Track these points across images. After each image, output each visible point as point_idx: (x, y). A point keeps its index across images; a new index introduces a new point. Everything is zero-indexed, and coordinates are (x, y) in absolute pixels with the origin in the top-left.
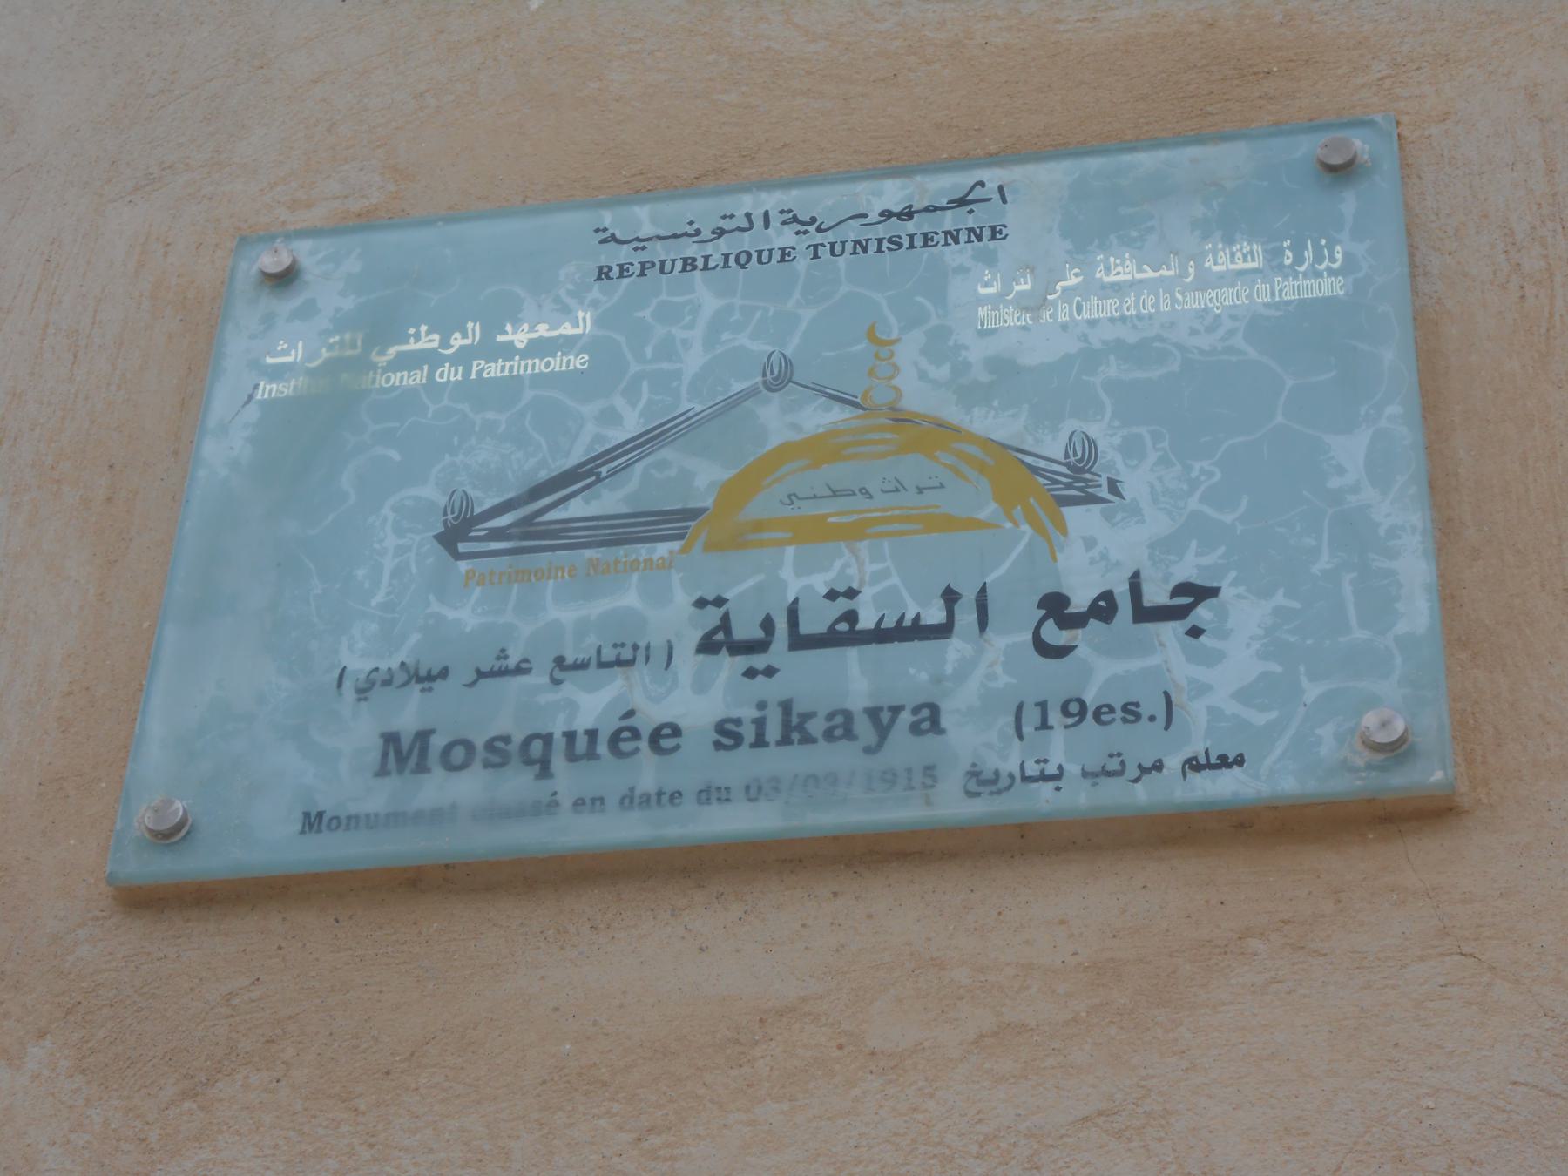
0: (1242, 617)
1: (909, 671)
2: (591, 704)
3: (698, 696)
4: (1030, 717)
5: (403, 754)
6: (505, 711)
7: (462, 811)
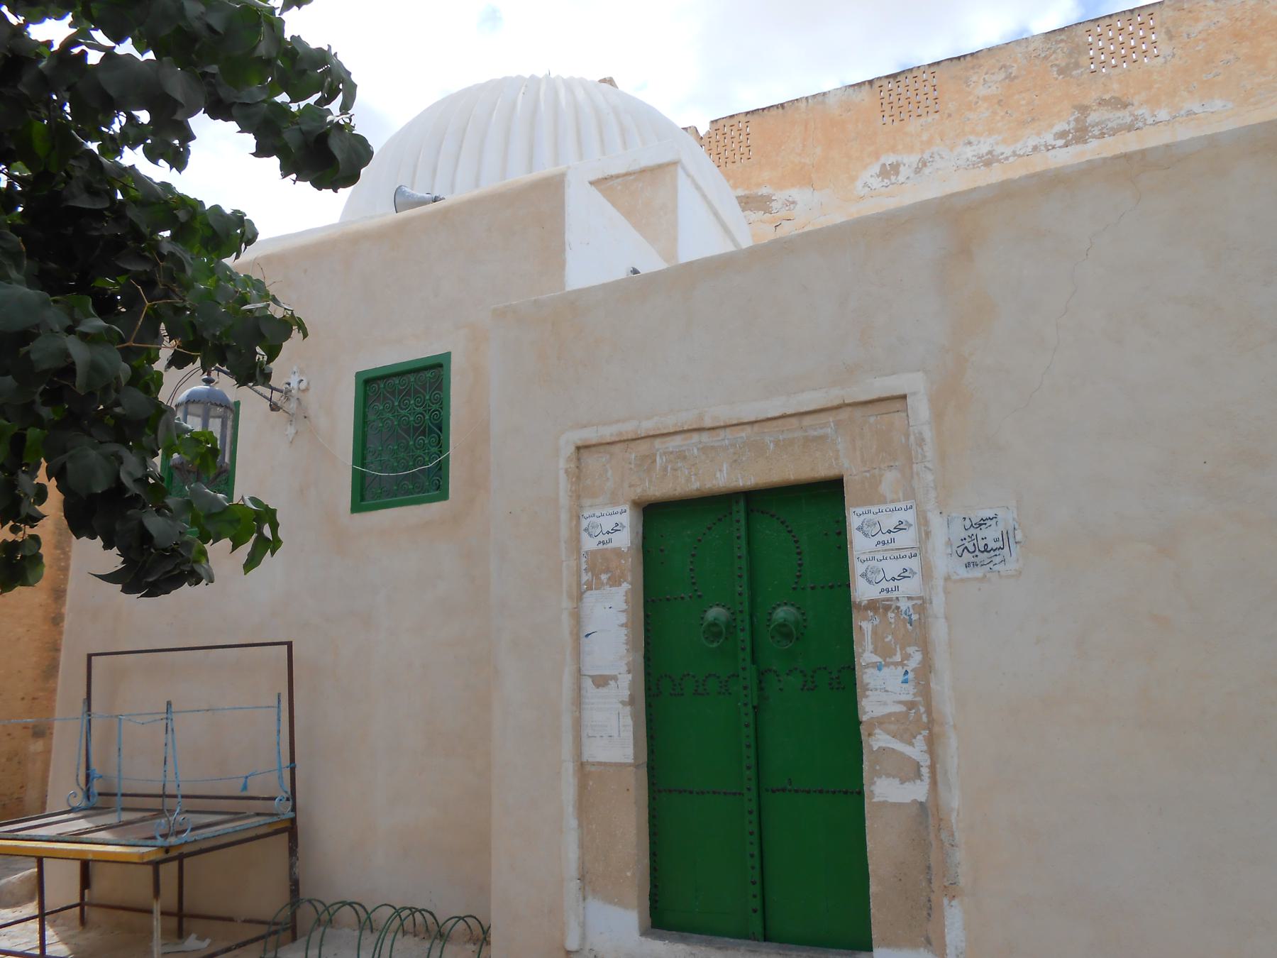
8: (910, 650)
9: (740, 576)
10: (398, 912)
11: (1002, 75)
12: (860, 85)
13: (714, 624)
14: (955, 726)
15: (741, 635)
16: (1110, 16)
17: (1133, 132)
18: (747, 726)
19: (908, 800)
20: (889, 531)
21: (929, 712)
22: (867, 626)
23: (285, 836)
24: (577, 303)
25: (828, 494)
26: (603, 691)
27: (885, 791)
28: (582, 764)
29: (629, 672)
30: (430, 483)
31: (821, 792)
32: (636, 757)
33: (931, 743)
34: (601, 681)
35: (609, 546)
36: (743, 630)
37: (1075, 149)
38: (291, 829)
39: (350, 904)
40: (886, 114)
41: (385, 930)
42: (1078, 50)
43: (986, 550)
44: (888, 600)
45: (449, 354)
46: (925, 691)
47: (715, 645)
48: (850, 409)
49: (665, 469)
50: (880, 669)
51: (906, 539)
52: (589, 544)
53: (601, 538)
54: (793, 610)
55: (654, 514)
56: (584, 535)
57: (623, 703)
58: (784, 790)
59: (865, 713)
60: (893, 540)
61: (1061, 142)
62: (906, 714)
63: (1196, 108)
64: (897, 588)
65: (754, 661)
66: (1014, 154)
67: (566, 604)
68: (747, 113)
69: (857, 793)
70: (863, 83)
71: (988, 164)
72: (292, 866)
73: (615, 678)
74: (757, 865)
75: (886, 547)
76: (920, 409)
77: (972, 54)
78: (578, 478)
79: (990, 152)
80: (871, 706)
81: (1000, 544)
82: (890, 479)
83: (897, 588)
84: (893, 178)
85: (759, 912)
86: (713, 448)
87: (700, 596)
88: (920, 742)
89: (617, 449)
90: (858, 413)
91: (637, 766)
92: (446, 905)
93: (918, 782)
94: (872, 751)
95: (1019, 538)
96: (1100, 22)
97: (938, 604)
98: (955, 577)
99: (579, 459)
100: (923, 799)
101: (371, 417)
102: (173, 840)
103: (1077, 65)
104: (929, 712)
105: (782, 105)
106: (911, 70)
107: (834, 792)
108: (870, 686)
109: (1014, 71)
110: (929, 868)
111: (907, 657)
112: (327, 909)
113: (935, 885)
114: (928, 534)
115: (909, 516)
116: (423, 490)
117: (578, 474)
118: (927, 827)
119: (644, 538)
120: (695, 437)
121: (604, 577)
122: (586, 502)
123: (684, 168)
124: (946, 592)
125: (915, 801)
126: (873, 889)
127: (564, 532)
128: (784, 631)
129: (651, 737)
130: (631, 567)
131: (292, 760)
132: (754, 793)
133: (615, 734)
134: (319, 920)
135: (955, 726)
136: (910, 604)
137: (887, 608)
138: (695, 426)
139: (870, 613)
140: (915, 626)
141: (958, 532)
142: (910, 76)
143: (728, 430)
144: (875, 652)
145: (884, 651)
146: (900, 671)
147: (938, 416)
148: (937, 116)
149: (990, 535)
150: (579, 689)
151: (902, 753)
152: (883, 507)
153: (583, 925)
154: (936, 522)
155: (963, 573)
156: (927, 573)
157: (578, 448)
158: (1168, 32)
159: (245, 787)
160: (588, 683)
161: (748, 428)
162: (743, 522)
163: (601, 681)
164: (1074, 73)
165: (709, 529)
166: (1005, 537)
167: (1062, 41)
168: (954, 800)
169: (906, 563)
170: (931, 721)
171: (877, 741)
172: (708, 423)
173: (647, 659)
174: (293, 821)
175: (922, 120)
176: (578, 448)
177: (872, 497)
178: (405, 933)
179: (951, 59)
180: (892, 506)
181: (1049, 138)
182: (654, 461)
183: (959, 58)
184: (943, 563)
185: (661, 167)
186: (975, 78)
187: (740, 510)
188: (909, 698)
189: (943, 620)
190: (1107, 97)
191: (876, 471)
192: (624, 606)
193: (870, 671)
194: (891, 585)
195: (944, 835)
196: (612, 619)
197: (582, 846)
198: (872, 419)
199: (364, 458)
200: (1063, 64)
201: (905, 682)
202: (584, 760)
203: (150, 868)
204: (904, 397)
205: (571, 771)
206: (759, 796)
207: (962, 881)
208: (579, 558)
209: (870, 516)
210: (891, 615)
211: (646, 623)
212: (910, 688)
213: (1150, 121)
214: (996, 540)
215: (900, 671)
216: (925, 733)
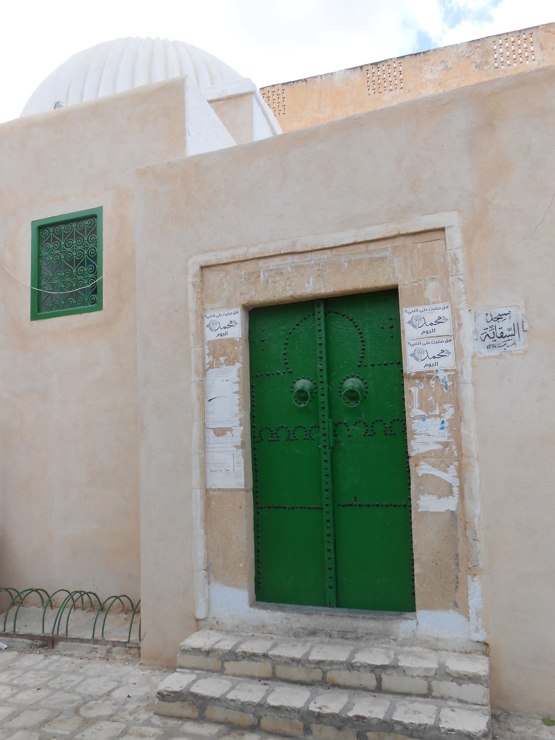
8: (446, 406)
9: (321, 358)
10: (71, 595)
11: (442, 67)
12: (354, 69)
13: (301, 391)
14: (478, 459)
15: (321, 399)
16: (507, 33)
18: (326, 461)
19: (443, 510)
20: (432, 324)
21: (460, 448)
22: (415, 390)
24: (200, 164)
25: (389, 296)
26: (221, 439)
27: (426, 504)
28: (207, 490)
29: (241, 425)
30: (88, 297)
31: (378, 505)
32: (246, 485)
33: (460, 470)
34: (220, 432)
35: (226, 337)
36: (322, 395)
39: (36, 591)
40: (371, 88)
41: (64, 606)
42: (488, 53)
43: (502, 337)
44: (430, 372)
45: (101, 208)
46: (456, 434)
47: (303, 405)
48: (403, 238)
49: (267, 282)
50: (424, 420)
51: (443, 329)
52: (210, 336)
53: (220, 331)
54: (358, 380)
55: (257, 314)
56: (207, 330)
57: (236, 447)
58: (351, 505)
59: (413, 450)
60: (434, 330)
62: (443, 450)
64: (437, 364)
65: (330, 416)
67: (194, 378)
68: (283, 84)
69: (407, 506)
70: (357, 67)
73: (230, 429)
74: (333, 557)
75: (429, 335)
76: (455, 238)
77: (424, 52)
78: (202, 289)
80: (417, 446)
81: (512, 332)
82: (432, 287)
83: (437, 364)
85: (334, 589)
86: (302, 266)
87: (291, 372)
88: (452, 470)
89: (230, 268)
90: (409, 241)
91: (246, 491)
92: (106, 590)
93: (451, 497)
94: (417, 477)
95: (526, 328)
96: (501, 37)
97: (467, 374)
98: (479, 355)
99: (202, 276)
100: (453, 509)
101: (44, 254)
103: (487, 63)
105: (305, 80)
106: (386, 61)
107: (387, 506)
108: (417, 432)
109: (449, 64)
110: (457, 555)
111: (443, 411)
112: (19, 595)
113: (461, 568)
114: (460, 325)
115: (446, 313)
116: (84, 303)
117: (201, 286)
118: (456, 528)
119: (250, 332)
120: (289, 259)
121: (222, 359)
122: (208, 306)
124: (473, 366)
125: (448, 511)
126: (417, 570)
127: (192, 328)
128: (352, 395)
129: (255, 471)
132: (330, 508)
133: (231, 469)
134: (14, 602)
135: (478, 459)
136: (446, 374)
137: (429, 378)
138: (289, 251)
139: (417, 381)
140: (450, 390)
141: (482, 323)
142: (386, 64)
143: (314, 253)
144: (421, 408)
145: (427, 407)
146: (439, 421)
147: (468, 242)
148: (402, 91)
149: (505, 325)
151: (439, 478)
152: (427, 307)
153: (208, 602)
154: (466, 317)
155: (486, 353)
156: (459, 353)
157: (202, 268)
160: (211, 434)
161: (329, 252)
162: (323, 319)
163: (220, 432)
164: (485, 68)
165: (298, 325)
166: (516, 327)
167: (478, 47)
168: (476, 509)
169: (444, 346)
170: (461, 455)
171: (421, 470)
172: (299, 248)
173: (253, 416)
175: (392, 93)
176: (202, 268)
177: (419, 300)
178: (75, 607)
179: (411, 55)
180: (433, 307)
182: (259, 276)
183: (416, 54)
184: (471, 345)
185: (241, 96)
186: (425, 68)
187: (320, 312)
188: (445, 439)
189: (471, 385)
191: (422, 282)
192: (237, 379)
193: (417, 421)
194: (433, 361)
195: (469, 533)
197: (207, 547)
198: (419, 245)
199: (39, 282)
200: (479, 62)
201: (442, 428)
202: (208, 487)
204: (443, 229)
205: (199, 496)
206: (334, 510)
207: (481, 564)
208: (203, 346)
209: (416, 314)
210: (432, 382)
211: (252, 392)
212: (445, 432)
214: (509, 330)
215: (439, 421)
216: (456, 463)
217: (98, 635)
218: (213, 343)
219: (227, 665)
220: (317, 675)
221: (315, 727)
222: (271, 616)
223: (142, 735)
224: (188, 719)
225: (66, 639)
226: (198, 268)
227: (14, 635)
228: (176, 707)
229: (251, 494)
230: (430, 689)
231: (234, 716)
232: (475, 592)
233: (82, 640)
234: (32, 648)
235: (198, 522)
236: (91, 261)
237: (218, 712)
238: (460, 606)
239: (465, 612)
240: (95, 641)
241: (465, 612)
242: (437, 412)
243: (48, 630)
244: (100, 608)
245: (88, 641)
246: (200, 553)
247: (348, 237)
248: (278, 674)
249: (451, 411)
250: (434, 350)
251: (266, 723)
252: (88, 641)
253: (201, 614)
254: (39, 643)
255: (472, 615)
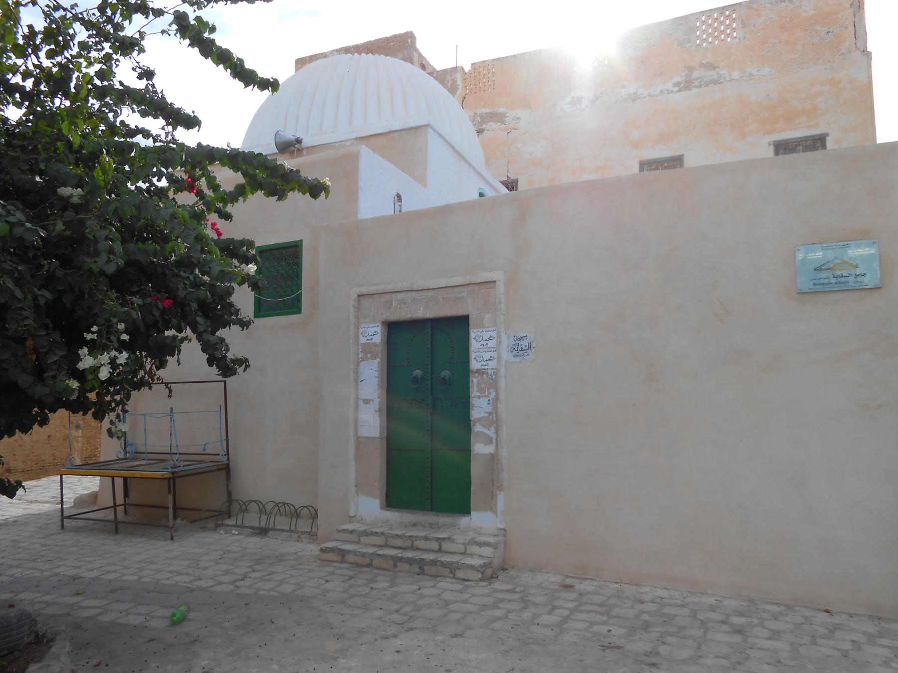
0: (868, 276)
1: (847, 279)
2: (826, 281)
3: (834, 281)
4: (855, 282)
5: (815, 284)
6: (821, 281)
7: (819, 288)
8: (491, 391)
10: (277, 504)
13: (415, 378)
17: (717, 86)
21: (497, 417)
22: (475, 380)
23: (224, 472)
25: (462, 322)
26: (368, 406)
27: (480, 449)
30: (293, 306)
34: (367, 402)
37: (684, 93)
38: (226, 469)
41: (270, 514)
46: (496, 408)
51: (491, 344)
52: (363, 340)
55: (393, 328)
56: (361, 336)
61: (676, 89)
63: (755, 72)
66: (649, 94)
67: (352, 367)
71: (634, 100)
72: (228, 486)
73: (372, 400)
76: (501, 287)
79: (635, 93)
82: (488, 317)
84: (578, 106)
88: (493, 429)
89: (376, 297)
97: (502, 372)
102: (176, 470)
104: (497, 417)
111: (490, 393)
114: (500, 342)
115: (494, 334)
117: (358, 308)
120: (410, 294)
121: (369, 355)
123: (432, 128)
130: (381, 352)
131: (227, 436)
137: (483, 373)
140: (493, 382)
145: (481, 391)
149: (524, 343)
150: (357, 405)
154: (504, 337)
155: (513, 359)
157: (359, 296)
158: (743, 23)
159: (204, 450)
160: (361, 402)
166: (530, 344)
168: (504, 453)
169: (492, 354)
170: (497, 420)
171: (477, 428)
174: (228, 465)
176: (359, 296)
177: (480, 325)
181: (669, 85)
184: (506, 355)
185: (419, 127)
190: (704, 62)
194: (485, 363)
196: (372, 373)
203: (166, 482)
213: (728, 78)
217: (293, 528)
218: (364, 344)
219: (362, 539)
220: (408, 543)
221: (399, 564)
222: (392, 515)
223: (349, 669)
224: (336, 562)
225: (274, 529)
226: (356, 296)
227: (243, 526)
228: (329, 556)
229: (385, 440)
230: (466, 550)
231: (359, 560)
232: (501, 500)
233: (283, 530)
234: (253, 535)
235: (352, 457)
236: (295, 277)
237: (351, 558)
238: (492, 509)
239: (496, 513)
240: (291, 531)
241: (496, 513)
242: (486, 394)
243: (263, 524)
244: (295, 514)
245: (287, 531)
246: (352, 476)
247: (443, 282)
248: (389, 543)
249: (494, 394)
250: (486, 356)
251: (376, 562)
252: (287, 531)
253: (352, 514)
254: (257, 531)
255: (499, 514)
